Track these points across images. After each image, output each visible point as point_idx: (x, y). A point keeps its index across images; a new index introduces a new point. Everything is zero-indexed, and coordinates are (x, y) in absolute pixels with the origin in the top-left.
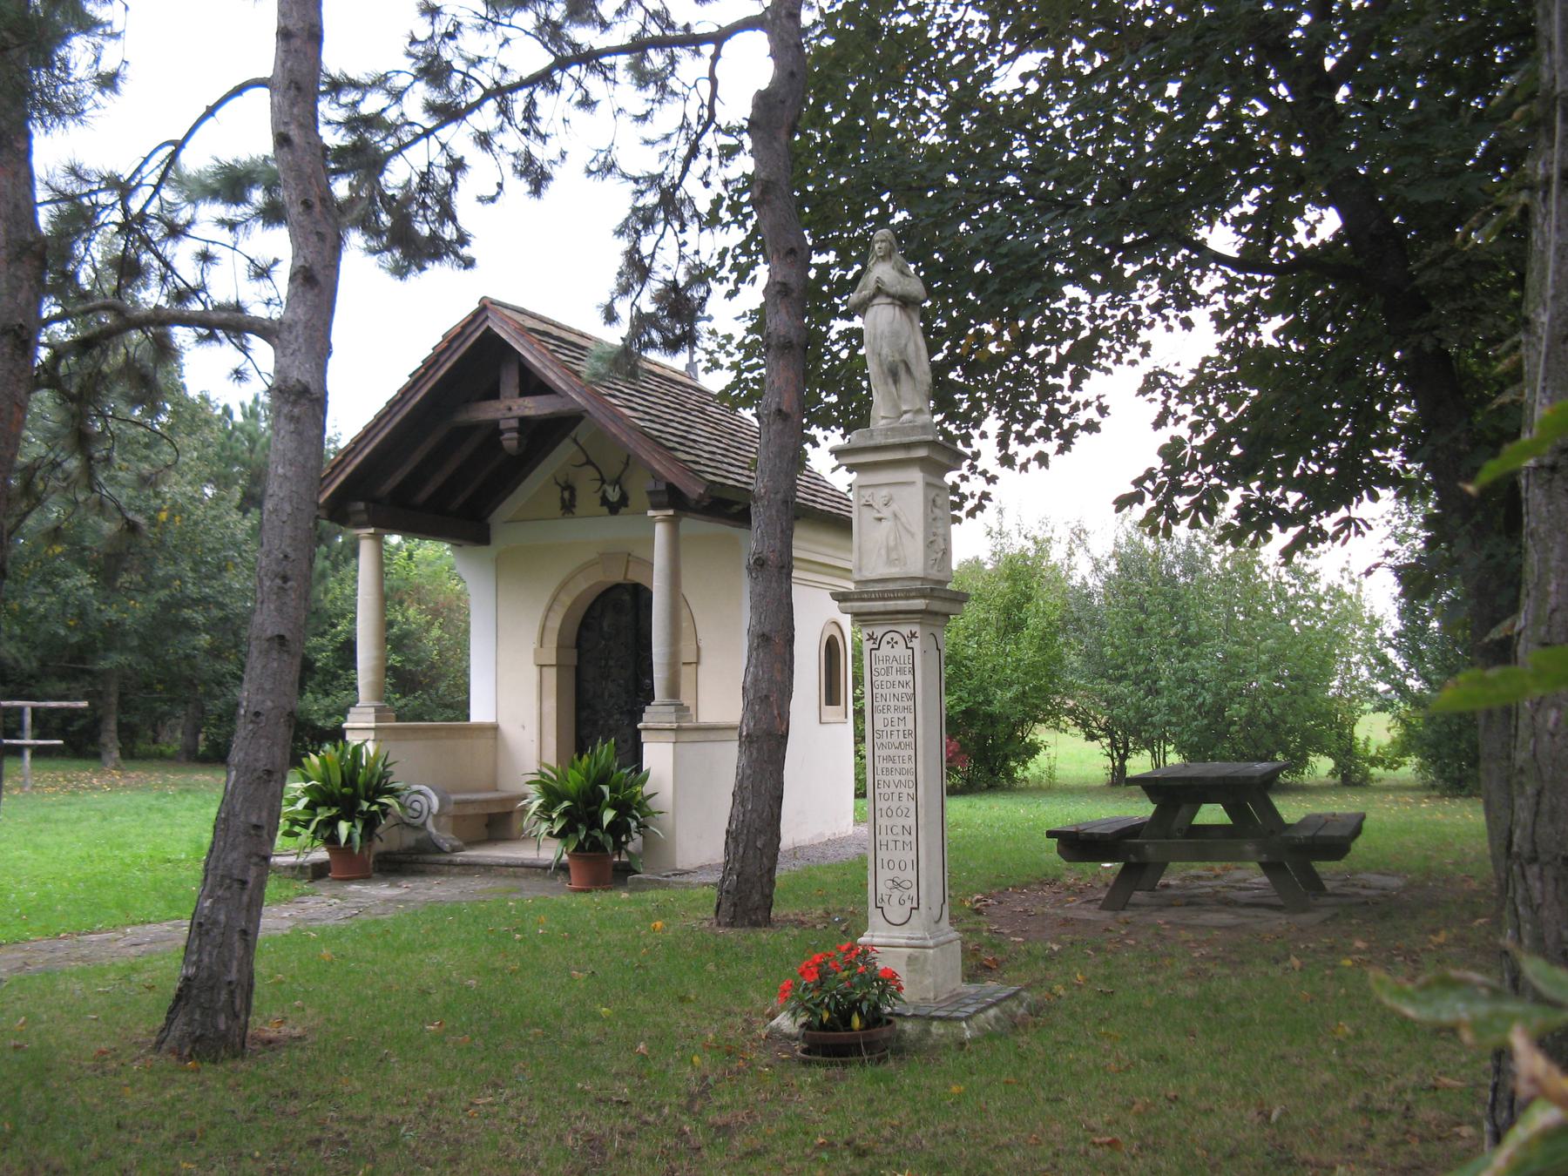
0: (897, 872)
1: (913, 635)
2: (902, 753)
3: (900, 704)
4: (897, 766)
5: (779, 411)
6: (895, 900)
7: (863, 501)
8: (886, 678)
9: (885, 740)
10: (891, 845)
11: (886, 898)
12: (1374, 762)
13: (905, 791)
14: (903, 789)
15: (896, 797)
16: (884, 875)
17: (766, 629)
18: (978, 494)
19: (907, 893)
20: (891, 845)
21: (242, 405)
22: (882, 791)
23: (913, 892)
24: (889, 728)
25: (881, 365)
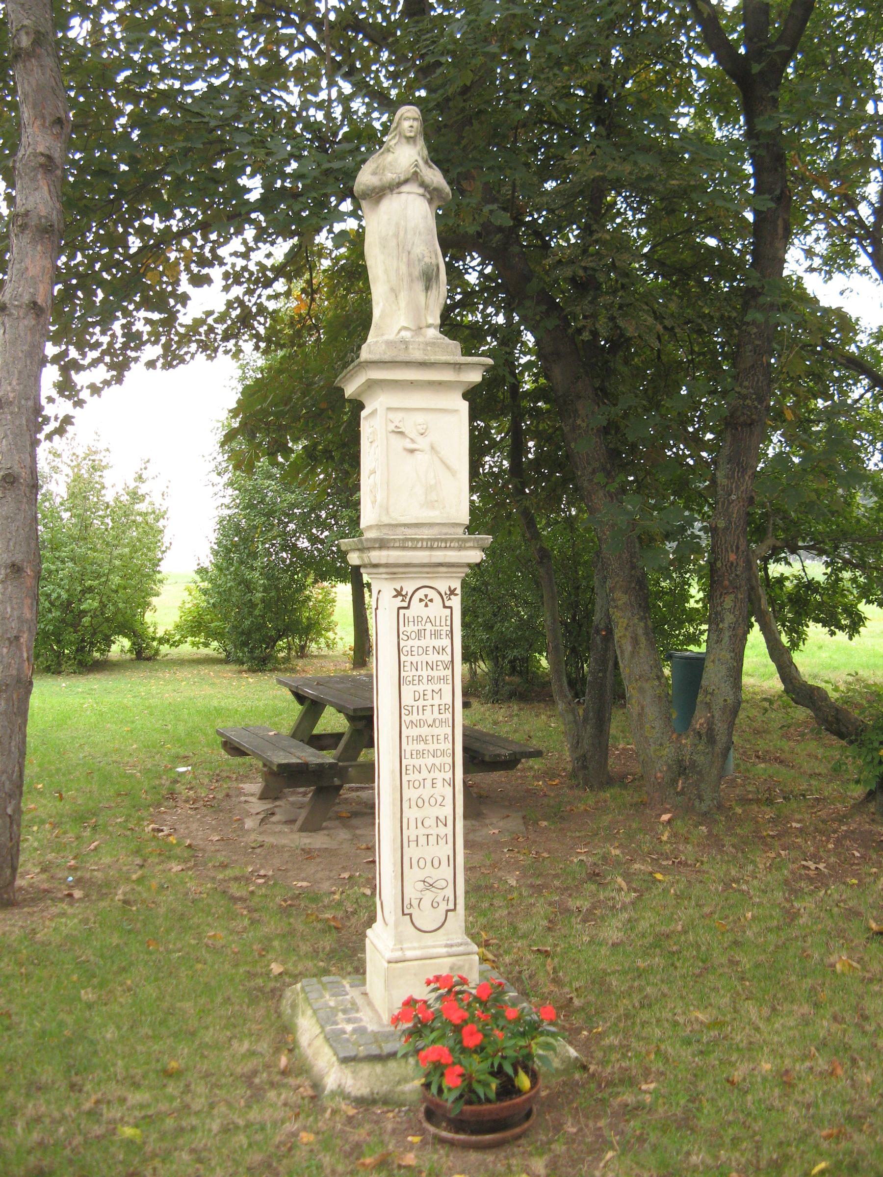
0: (428, 871)
1: (452, 592)
2: (435, 731)
3: (435, 673)
4: (431, 747)
5: (35, 303)
6: (426, 903)
7: (392, 427)
8: (416, 643)
9: (415, 717)
10: (422, 840)
11: (415, 903)
12: (161, 641)
14: (436, 774)
15: (428, 783)
17: (18, 558)
18: (61, 417)
19: (442, 894)
20: (422, 840)
22: (411, 777)
23: (449, 892)
24: (421, 703)
25: (409, 264)
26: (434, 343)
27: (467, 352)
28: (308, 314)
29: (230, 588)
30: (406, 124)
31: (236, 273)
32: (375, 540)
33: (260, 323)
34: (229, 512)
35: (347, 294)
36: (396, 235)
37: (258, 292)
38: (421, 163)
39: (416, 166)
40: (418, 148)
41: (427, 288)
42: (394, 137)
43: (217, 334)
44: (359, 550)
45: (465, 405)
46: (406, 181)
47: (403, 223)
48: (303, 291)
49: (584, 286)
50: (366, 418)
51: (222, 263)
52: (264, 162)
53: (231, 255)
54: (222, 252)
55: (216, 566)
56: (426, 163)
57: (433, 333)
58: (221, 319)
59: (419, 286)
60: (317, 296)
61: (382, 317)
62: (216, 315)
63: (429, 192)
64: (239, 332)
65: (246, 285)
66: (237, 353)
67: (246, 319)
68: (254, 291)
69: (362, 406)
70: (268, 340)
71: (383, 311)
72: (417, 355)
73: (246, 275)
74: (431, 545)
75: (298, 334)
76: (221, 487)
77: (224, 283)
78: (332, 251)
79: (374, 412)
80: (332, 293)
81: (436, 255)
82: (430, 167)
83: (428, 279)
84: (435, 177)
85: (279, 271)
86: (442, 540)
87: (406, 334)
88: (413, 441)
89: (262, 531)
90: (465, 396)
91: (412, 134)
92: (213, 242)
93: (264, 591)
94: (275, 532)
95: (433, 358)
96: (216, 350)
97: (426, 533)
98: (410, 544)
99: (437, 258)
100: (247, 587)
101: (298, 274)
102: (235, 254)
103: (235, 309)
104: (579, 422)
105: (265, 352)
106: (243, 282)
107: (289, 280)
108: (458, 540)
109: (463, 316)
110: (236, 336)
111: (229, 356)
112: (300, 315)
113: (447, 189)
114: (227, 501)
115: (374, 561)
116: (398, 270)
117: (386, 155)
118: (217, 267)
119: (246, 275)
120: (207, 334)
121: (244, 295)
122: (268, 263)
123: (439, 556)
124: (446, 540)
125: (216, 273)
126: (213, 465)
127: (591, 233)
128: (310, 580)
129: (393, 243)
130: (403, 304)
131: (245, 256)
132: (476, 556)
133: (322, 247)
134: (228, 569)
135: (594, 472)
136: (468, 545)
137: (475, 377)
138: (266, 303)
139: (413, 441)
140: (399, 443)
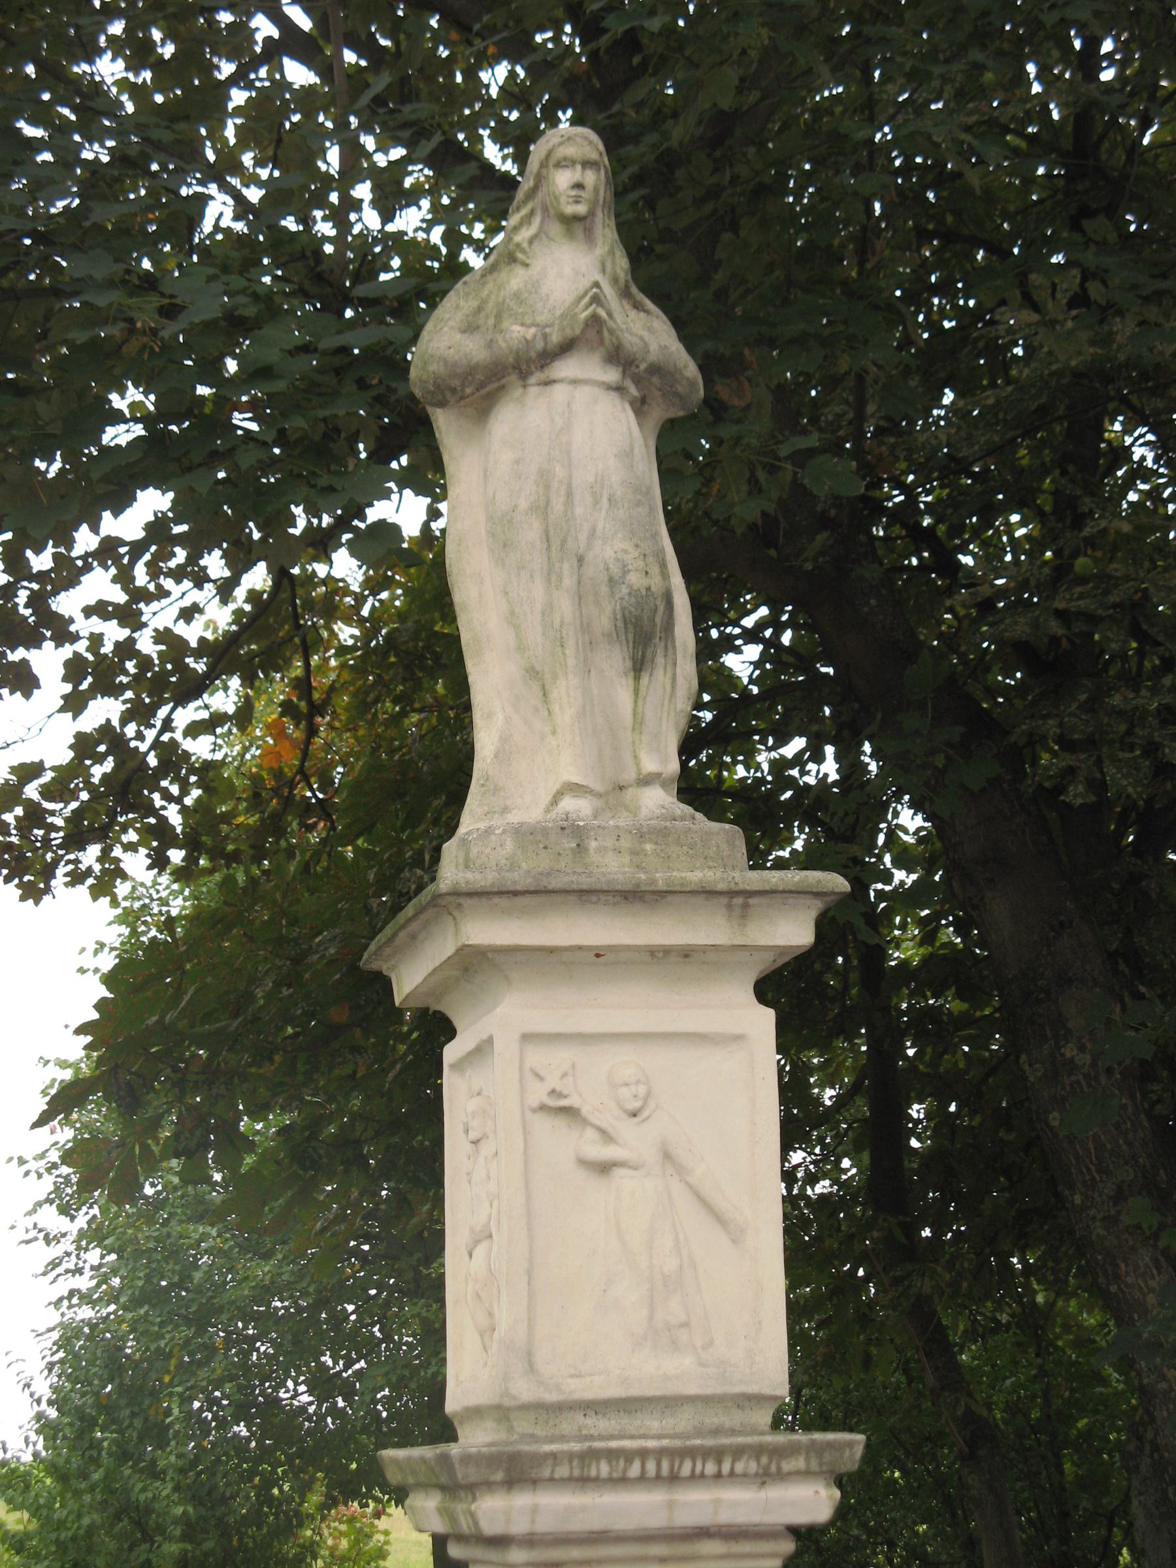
7: (538, 1094)
26: (664, 833)
27: (757, 858)
28: (301, 771)
29: (91, 1531)
30: (563, 179)
31: (101, 658)
32: (491, 1460)
33: (167, 796)
34: (86, 1313)
35: (404, 714)
36: (542, 509)
37: (163, 712)
38: (608, 291)
39: (596, 300)
40: (600, 250)
41: (639, 666)
42: (527, 220)
43: (53, 828)
44: (443, 1488)
45: (768, 1016)
46: (567, 347)
47: (560, 471)
48: (288, 708)
49: (1055, 665)
50: (458, 1066)
51: (63, 633)
52: (154, 332)
53: (88, 612)
54: (67, 604)
55: (52, 1468)
56: (625, 294)
57: (658, 801)
58: (59, 790)
59: (613, 661)
60: (322, 721)
61: (500, 755)
62: (48, 776)
63: (637, 381)
64: (113, 820)
65: (129, 694)
66: (112, 874)
67: (130, 787)
68: (152, 710)
69: (449, 1032)
70: (192, 844)
71: (505, 739)
72: (611, 865)
73: (130, 666)
74: (674, 1466)
75: (274, 825)
76: (67, 1245)
77: (68, 688)
78: (360, 600)
79: (483, 1049)
80: (363, 706)
81: (663, 565)
82: (637, 306)
83: (641, 637)
84: (652, 333)
85: (223, 655)
86: (706, 1453)
87: (578, 807)
88: (606, 1136)
89: (181, 1364)
90: (765, 991)
91: (581, 209)
92: (41, 577)
93: (185, 1537)
94: (218, 1367)
95: (661, 879)
96: (48, 872)
97: (654, 1431)
98: (604, 1469)
99: (665, 575)
100: (139, 1524)
101: (272, 660)
102: (99, 610)
103: (100, 759)
104: (1069, 1051)
105: (182, 875)
106: (122, 688)
107: (249, 680)
108: (758, 1451)
109: (723, 766)
110: (104, 834)
111: (82, 891)
112: (278, 774)
113: (691, 369)
114: (84, 1283)
115: (489, 1528)
116: (548, 609)
117: (503, 275)
118: (48, 645)
119: (130, 666)
120: (25, 826)
121: (124, 721)
122: (192, 633)
123: (698, 1504)
124: (718, 1454)
125: (47, 661)
126: (47, 1184)
127: (1079, 521)
128: (315, 1499)
129: (532, 532)
130: (565, 715)
131: (128, 616)
132: (813, 1502)
133: (336, 587)
134: (84, 1475)
135: (1119, 1197)
136: (787, 1466)
137: (795, 931)
138: (188, 745)
139: (606, 1136)
140: (560, 1144)
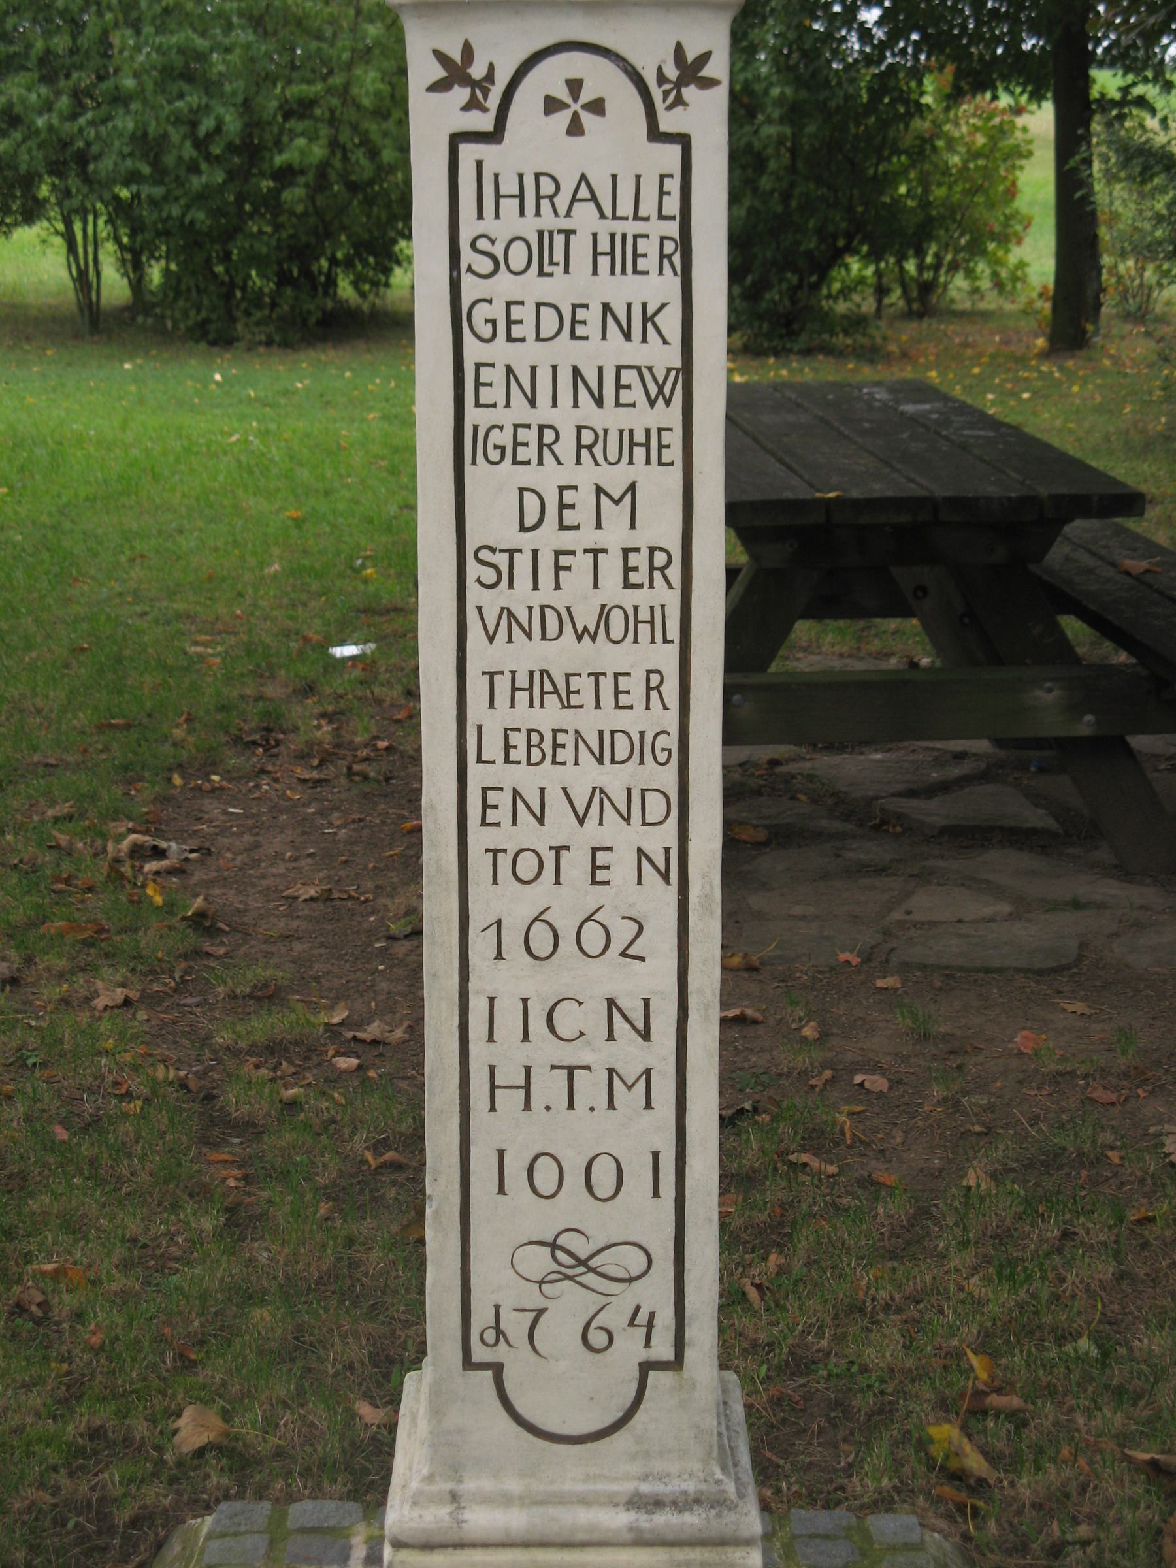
1: (691, 71)
3: (610, 419)
4: (589, 722)
6: (560, 1331)
8: (532, 288)
10: (549, 1087)
11: (515, 1325)
13: (624, 839)
14: (613, 831)
15: (576, 865)
16: (508, 1227)
19: (625, 1299)
20: (549, 1087)
21: (644, 306)
22: (506, 837)
23: (656, 1292)
24: (548, 538)
